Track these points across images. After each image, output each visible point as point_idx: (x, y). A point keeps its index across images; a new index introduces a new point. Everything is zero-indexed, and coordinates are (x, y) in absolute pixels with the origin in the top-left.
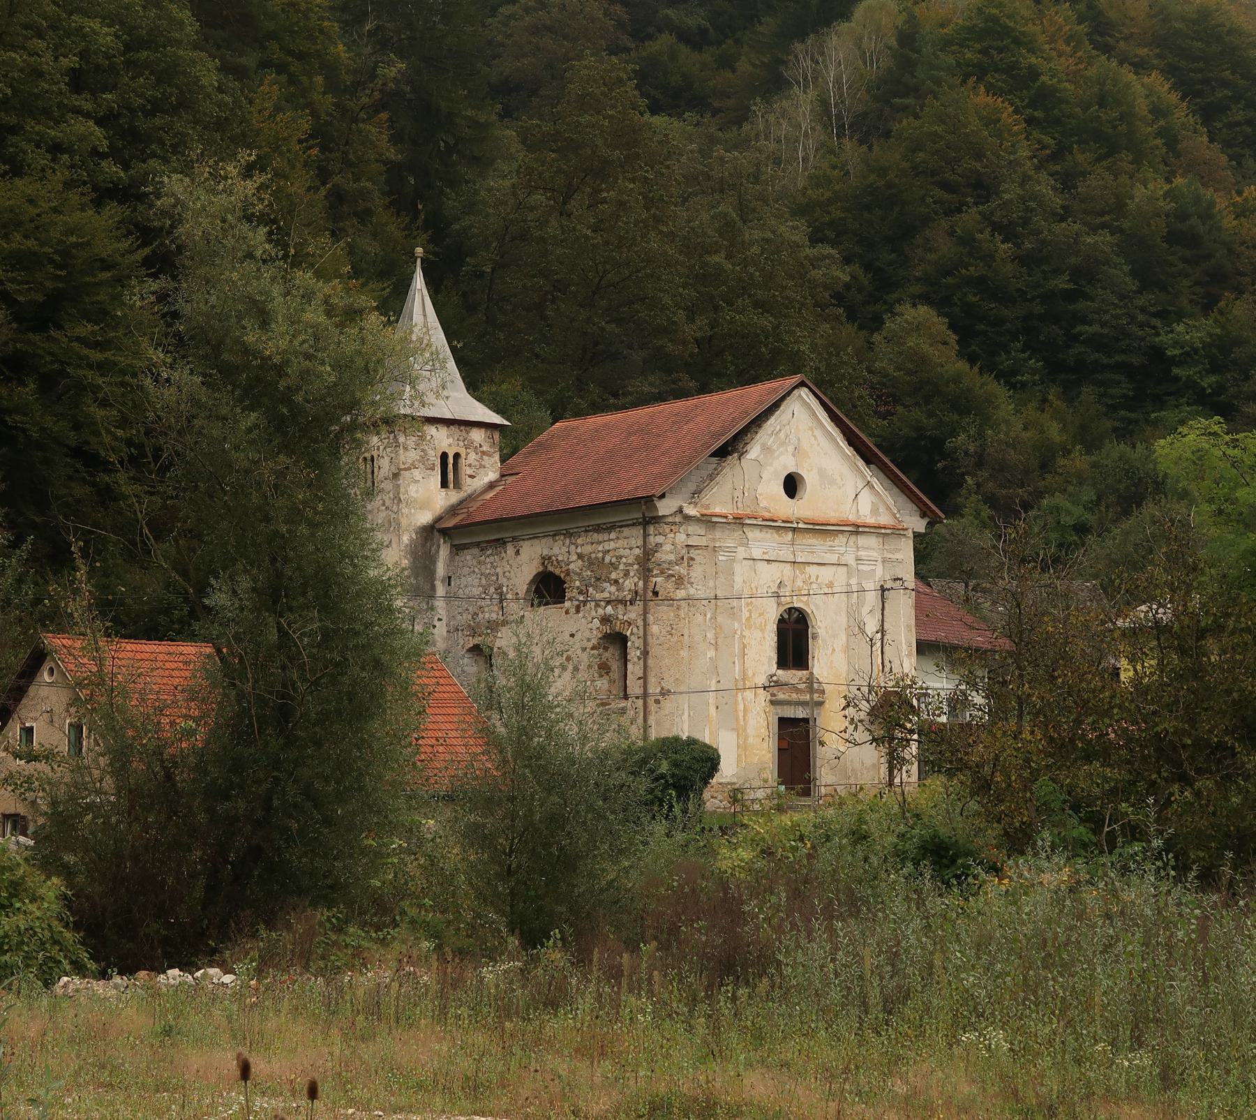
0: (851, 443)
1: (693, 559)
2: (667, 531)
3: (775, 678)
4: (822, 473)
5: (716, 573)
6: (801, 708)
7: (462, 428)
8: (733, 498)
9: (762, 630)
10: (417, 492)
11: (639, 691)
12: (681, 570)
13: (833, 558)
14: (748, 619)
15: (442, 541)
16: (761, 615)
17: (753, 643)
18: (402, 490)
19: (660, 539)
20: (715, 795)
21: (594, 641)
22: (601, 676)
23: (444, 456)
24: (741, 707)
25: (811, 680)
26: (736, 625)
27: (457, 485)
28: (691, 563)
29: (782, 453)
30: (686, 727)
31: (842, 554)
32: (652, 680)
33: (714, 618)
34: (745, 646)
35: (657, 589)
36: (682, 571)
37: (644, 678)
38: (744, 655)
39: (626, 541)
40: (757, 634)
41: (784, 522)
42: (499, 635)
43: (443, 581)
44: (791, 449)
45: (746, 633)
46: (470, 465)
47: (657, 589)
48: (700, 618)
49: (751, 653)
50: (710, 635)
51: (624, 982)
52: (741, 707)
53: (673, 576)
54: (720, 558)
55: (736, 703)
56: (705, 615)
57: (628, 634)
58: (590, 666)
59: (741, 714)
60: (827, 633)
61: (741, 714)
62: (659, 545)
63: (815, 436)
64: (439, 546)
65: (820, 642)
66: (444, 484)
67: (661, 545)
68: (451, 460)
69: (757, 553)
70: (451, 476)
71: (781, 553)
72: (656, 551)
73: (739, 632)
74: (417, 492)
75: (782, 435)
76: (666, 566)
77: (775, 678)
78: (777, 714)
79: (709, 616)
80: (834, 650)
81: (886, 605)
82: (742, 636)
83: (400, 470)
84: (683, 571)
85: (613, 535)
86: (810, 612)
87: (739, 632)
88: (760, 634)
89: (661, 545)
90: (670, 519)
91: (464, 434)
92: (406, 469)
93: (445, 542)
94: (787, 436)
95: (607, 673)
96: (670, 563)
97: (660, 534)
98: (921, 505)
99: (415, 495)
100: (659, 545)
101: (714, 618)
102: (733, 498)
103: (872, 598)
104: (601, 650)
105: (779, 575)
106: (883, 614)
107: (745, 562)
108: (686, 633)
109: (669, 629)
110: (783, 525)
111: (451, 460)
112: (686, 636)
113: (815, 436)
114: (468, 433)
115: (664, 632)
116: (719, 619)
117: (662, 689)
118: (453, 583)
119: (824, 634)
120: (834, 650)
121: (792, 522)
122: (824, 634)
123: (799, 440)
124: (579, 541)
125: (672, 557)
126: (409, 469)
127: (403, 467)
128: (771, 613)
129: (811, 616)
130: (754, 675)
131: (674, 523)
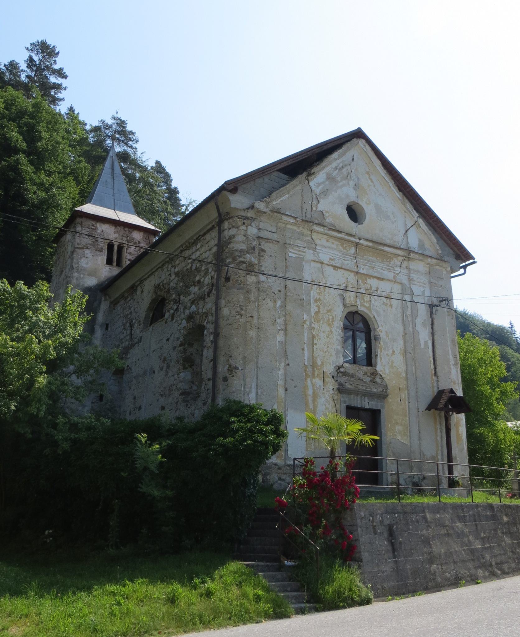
0: (400, 190)
1: (263, 251)
2: (240, 223)
3: (342, 370)
4: (378, 207)
5: (286, 267)
6: (367, 399)
7: (126, 229)
8: (302, 209)
9: (330, 325)
10: (87, 263)
11: (210, 374)
12: (251, 258)
13: (390, 276)
14: (317, 313)
15: (103, 298)
16: (328, 311)
17: (322, 335)
18: (75, 261)
19: (233, 232)
20: (283, 477)
21: (181, 339)
22: (185, 368)
23: (110, 246)
24: (310, 392)
25: (374, 374)
26: (305, 316)
27: (119, 264)
28: (262, 253)
29: (344, 185)
30: (253, 395)
31: (397, 274)
32: (222, 360)
33: (284, 306)
34: (313, 337)
35: (229, 275)
36: (253, 259)
37: (215, 360)
38: (313, 344)
39: (207, 245)
40: (325, 327)
41: (348, 234)
42: (129, 356)
43: (101, 326)
44: (352, 183)
45: (315, 325)
46: (130, 253)
47: (229, 275)
48: (270, 304)
49: (320, 344)
50: (280, 321)
51: (462, 257)
52: (310, 392)
53: (244, 262)
54: (291, 255)
55: (305, 388)
56: (275, 302)
57: (205, 323)
58: (177, 362)
59: (310, 399)
60: (388, 336)
61: (310, 399)
62: (232, 237)
63: (371, 180)
64: (100, 302)
65: (381, 343)
66: (109, 262)
67: (234, 236)
68: (116, 248)
69: (324, 258)
70: (115, 258)
71: (346, 262)
72: (230, 243)
73: (308, 323)
74: (87, 263)
75: (344, 171)
76: (238, 253)
77: (342, 370)
78: (345, 402)
79: (279, 303)
80: (394, 352)
81: (435, 321)
82: (311, 328)
83: (75, 248)
84: (254, 260)
85: (199, 246)
86: (372, 316)
87: (308, 323)
88: (328, 329)
89: (234, 236)
90: (243, 213)
91: (127, 233)
92: (79, 248)
93: (106, 300)
94: (348, 174)
95: (191, 366)
96: (241, 251)
97: (233, 227)
98: (456, 249)
99: (85, 266)
100: (232, 237)
101: (284, 306)
102: (302, 209)
103: (423, 310)
104: (186, 346)
105: (344, 280)
106: (432, 328)
107: (313, 264)
108: (255, 315)
109: (239, 309)
110: (347, 237)
111: (116, 248)
112: (255, 319)
113: (371, 180)
114: (130, 233)
115: (234, 312)
116: (289, 307)
117: (230, 366)
118: (109, 329)
119: (385, 337)
120: (394, 352)
121: (354, 236)
122: (385, 337)
123: (358, 179)
124: (177, 263)
125: (243, 247)
126: (82, 248)
127: (77, 246)
128: (339, 312)
129: (373, 320)
130: (323, 364)
131: (247, 218)
